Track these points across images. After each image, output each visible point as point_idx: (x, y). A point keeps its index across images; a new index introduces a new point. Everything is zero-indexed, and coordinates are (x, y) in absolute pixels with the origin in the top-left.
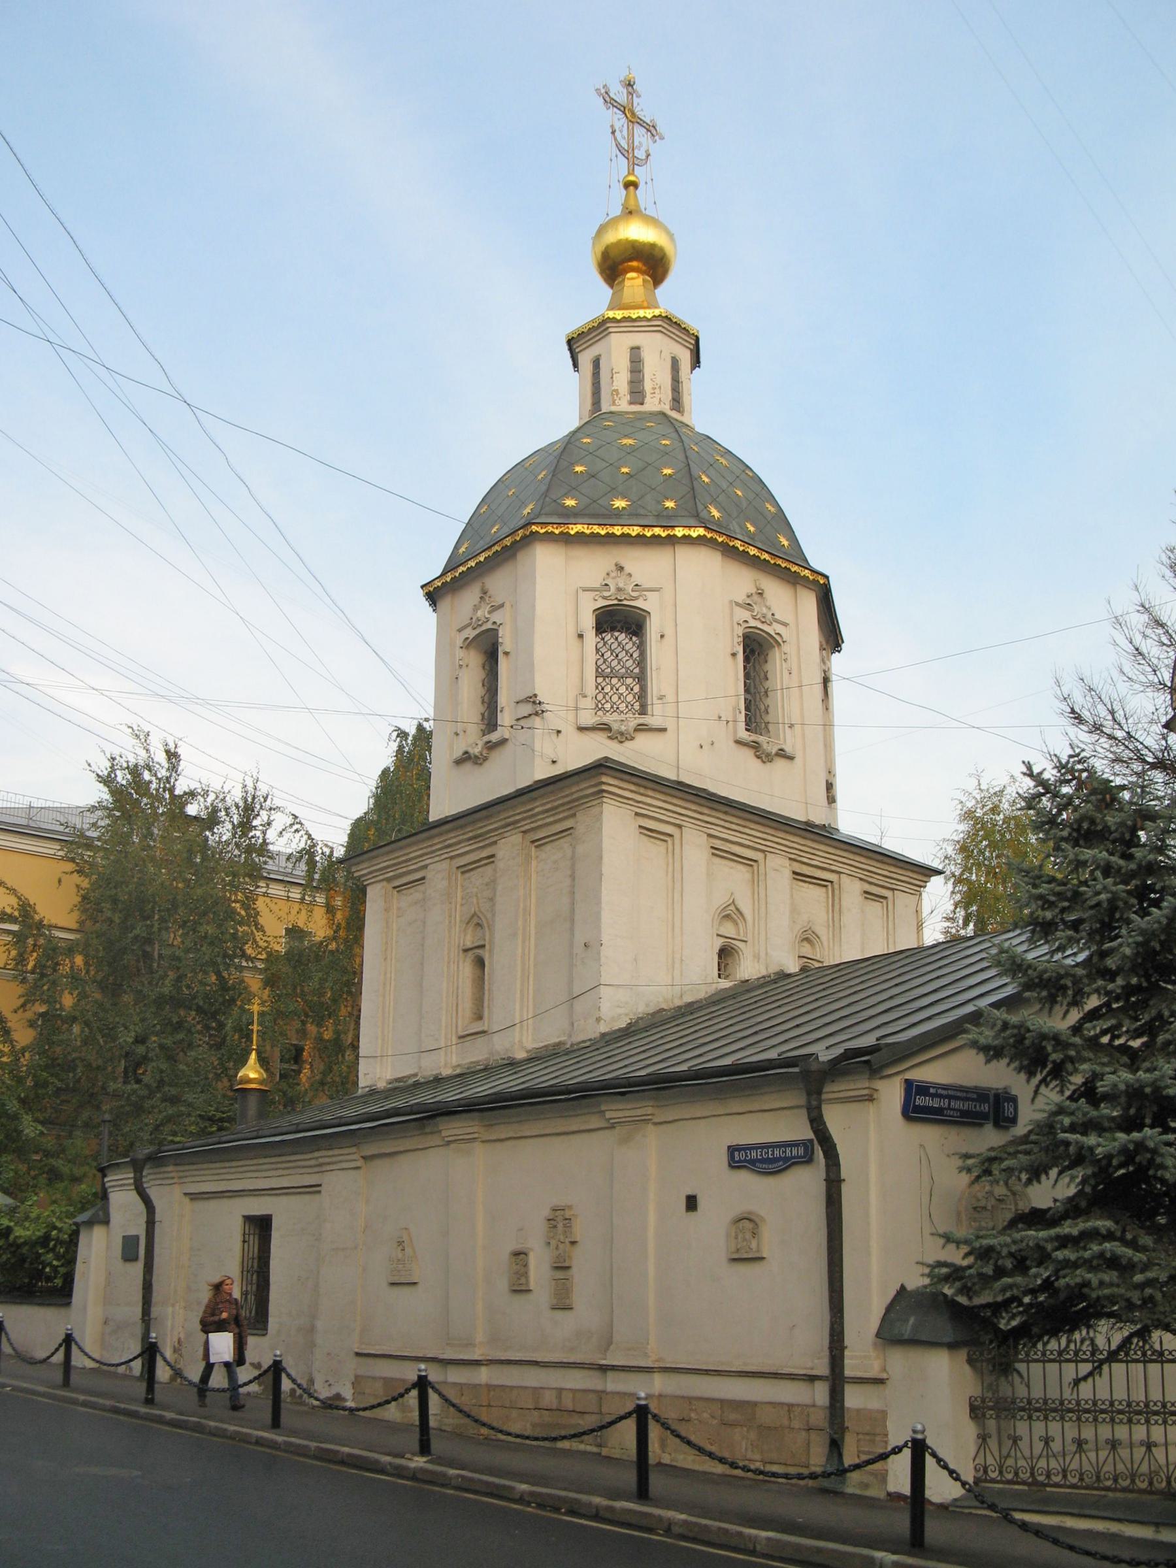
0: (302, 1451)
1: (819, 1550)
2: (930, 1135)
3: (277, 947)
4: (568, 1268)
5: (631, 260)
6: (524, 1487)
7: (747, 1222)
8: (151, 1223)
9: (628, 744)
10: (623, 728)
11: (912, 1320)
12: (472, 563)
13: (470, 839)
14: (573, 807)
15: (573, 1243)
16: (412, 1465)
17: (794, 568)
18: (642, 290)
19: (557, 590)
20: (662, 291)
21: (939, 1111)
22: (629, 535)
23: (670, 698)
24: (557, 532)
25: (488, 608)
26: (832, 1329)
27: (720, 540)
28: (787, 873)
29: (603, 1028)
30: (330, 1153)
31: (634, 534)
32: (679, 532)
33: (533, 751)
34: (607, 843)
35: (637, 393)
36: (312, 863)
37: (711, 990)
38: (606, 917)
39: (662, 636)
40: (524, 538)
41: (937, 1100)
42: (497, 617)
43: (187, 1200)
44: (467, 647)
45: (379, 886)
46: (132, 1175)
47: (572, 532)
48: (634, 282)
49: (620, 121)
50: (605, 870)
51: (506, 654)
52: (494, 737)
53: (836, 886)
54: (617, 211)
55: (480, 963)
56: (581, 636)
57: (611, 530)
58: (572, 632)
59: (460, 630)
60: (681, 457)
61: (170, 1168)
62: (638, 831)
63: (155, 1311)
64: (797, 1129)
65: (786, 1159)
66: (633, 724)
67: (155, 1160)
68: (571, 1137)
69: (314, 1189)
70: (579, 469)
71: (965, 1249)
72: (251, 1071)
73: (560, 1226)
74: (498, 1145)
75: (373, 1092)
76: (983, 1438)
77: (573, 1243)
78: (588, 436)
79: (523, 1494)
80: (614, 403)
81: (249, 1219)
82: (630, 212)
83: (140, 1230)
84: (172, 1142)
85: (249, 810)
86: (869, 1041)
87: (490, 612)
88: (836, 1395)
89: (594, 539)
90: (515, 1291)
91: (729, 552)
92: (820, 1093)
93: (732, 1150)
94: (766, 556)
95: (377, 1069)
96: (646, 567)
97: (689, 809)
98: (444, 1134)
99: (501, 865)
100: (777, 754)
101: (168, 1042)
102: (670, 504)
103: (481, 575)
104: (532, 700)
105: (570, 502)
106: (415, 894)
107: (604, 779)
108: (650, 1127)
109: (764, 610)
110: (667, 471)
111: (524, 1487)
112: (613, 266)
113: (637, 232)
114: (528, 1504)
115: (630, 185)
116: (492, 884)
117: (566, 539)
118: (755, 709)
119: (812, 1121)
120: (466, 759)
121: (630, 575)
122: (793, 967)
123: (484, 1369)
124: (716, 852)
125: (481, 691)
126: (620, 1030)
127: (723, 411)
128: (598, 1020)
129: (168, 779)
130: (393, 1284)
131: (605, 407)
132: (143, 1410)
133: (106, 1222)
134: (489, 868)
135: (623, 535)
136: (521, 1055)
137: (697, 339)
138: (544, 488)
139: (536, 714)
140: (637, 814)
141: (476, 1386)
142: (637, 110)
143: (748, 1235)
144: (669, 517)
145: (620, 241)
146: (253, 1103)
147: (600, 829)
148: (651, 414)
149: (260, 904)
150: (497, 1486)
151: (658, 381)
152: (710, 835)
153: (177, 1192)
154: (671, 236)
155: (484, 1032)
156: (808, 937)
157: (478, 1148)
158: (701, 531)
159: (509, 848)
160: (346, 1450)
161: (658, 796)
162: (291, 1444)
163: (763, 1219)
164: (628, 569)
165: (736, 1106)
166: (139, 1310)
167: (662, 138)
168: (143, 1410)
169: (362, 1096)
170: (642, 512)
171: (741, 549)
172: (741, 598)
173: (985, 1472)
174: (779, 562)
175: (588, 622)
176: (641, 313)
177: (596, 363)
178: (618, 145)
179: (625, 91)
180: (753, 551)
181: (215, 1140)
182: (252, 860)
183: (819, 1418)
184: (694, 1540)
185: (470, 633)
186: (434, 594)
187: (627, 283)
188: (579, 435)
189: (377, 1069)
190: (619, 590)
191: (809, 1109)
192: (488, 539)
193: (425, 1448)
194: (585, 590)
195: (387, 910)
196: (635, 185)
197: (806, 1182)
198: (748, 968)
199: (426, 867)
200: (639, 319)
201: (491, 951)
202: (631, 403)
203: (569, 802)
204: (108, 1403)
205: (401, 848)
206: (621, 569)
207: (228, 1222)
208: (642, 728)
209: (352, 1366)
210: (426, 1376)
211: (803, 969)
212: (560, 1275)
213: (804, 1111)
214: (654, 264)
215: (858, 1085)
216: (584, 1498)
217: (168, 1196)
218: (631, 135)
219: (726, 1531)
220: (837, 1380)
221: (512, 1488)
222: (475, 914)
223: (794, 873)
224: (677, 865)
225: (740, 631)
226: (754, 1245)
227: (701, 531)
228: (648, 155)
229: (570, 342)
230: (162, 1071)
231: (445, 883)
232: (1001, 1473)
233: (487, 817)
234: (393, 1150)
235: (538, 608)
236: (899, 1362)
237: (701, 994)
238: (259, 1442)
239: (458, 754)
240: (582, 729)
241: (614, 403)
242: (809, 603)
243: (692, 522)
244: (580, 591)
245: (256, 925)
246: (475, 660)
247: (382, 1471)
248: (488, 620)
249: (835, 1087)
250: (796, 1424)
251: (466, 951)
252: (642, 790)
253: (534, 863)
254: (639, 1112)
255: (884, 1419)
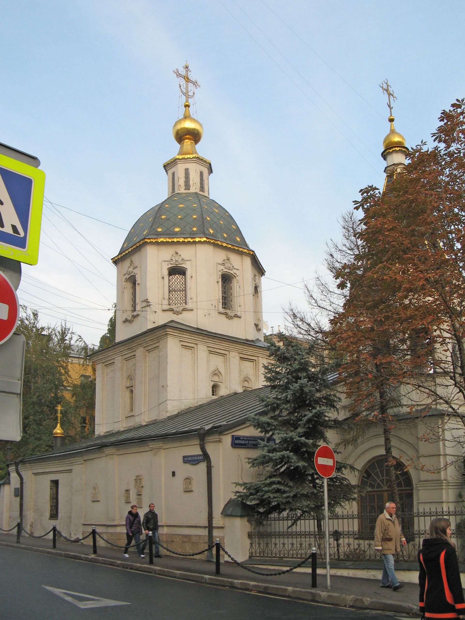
0: (60, 555)
1: (191, 576)
2: (243, 453)
3: (76, 383)
4: (141, 495)
5: (186, 135)
6: (119, 562)
7: (188, 480)
8: (22, 483)
9: (180, 315)
10: (178, 310)
11: (231, 509)
12: (127, 252)
13: (127, 349)
14: (159, 339)
15: (142, 487)
16: (90, 557)
17: (241, 249)
18: (190, 146)
19: (155, 261)
20: (198, 147)
21: (245, 445)
22: (179, 241)
23: (194, 299)
24: (154, 241)
25: (132, 268)
26: (20, 503)
27: (212, 242)
28: (238, 358)
29: (168, 414)
30: (74, 459)
31: (181, 241)
32: (197, 240)
33: (147, 319)
34: (169, 352)
35: (187, 186)
36: (86, 352)
37: (209, 400)
38: (169, 377)
39: (191, 277)
40: (143, 243)
41: (243, 441)
42: (135, 271)
43: (33, 475)
44: (127, 281)
45: (100, 365)
46: (15, 467)
47: (159, 241)
48: (187, 143)
49: (183, 82)
50: (169, 361)
51: (139, 284)
52: (135, 313)
53: (257, 361)
54: (182, 117)
55: (132, 391)
56: (163, 278)
57: (173, 240)
58: (160, 277)
59: (124, 275)
60: (200, 211)
61: (27, 465)
62: (181, 347)
63: (24, 513)
64: (198, 451)
65: (198, 460)
66: (181, 308)
67: (23, 462)
68: (142, 453)
69: (70, 471)
70: (163, 217)
71: (243, 487)
72: (58, 430)
73: (138, 481)
74: (121, 456)
75: (100, 437)
76: (251, 544)
77: (142, 487)
78: (167, 204)
79: (119, 564)
80: (179, 190)
81: (52, 481)
82: (186, 117)
83: (19, 486)
84: (36, 455)
85: (63, 333)
86: (199, 427)
87: (133, 269)
88: (210, 532)
89: (167, 243)
90: (127, 503)
91: (216, 245)
92: (203, 440)
93: (184, 457)
94: (230, 246)
95: (101, 429)
96: (186, 253)
97: (199, 338)
98: (106, 452)
99: (137, 358)
100: (234, 316)
101: (37, 418)
102: (195, 229)
103: (130, 256)
104: (146, 301)
105: (160, 230)
106: (111, 368)
107: (167, 330)
108: (162, 450)
109: (229, 265)
110: (195, 217)
111: (119, 562)
112: (181, 136)
113: (188, 125)
114: (120, 567)
115: (187, 106)
116: (135, 365)
117: (157, 243)
118: (226, 301)
119: (201, 449)
120: (126, 321)
121: (180, 255)
122: (240, 390)
123: (118, 528)
124: (211, 352)
125: (132, 297)
126: (175, 415)
127: (220, 191)
128: (167, 412)
129: (34, 323)
130: (93, 501)
131: (177, 191)
132: (16, 545)
133: (9, 483)
134: (134, 360)
135: (177, 241)
136: (144, 424)
137: (210, 164)
138: (151, 224)
139: (148, 306)
140: (180, 341)
141: (116, 533)
142: (190, 77)
143: (188, 484)
144: (194, 234)
145: (182, 128)
146: (59, 441)
147: (167, 347)
148: (193, 193)
149: (70, 367)
150: (112, 562)
151: (195, 181)
152: (208, 346)
153: (30, 473)
154: (201, 125)
155: (133, 416)
156: (246, 380)
157: (115, 457)
158: (205, 239)
159: (140, 352)
160: (73, 554)
161: (187, 334)
162: (57, 553)
163: (192, 479)
164: (179, 253)
165: (185, 443)
166: (19, 513)
167: (199, 87)
168: (16, 545)
169: (96, 438)
170: (185, 232)
171: (220, 244)
172: (221, 261)
173: (252, 554)
174: (235, 248)
175: (166, 273)
176: (189, 156)
177: (173, 174)
178: (182, 91)
179: (185, 70)
180: (224, 245)
181: (52, 453)
182: (66, 350)
183: (206, 539)
184: (162, 575)
185: (127, 276)
186: (116, 261)
187: (185, 144)
188: (164, 204)
189: (101, 429)
190: (176, 261)
191: (200, 445)
192: (133, 242)
193: (95, 552)
194: (164, 261)
195: (103, 373)
196: (188, 106)
197: (203, 466)
198: (223, 392)
199: (114, 358)
200: (188, 158)
201: (135, 388)
202: (185, 189)
203: (158, 337)
204: (5, 543)
205: (106, 352)
206: (177, 253)
207: (46, 481)
208: (184, 310)
209: (81, 529)
210: (95, 530)
211: (245, 391)
212: (139, 497)
213: (199, 446)
214: (195, 136)
215: (215, 437)
216: (135, 564)
217: (27, 474)
218: (187, 87)
219: (169, 572)
220: (210, 527)
221: (116, 562)
222: (130, 375)
223: (241, 358)
224: (196, 358)
225: (220, 274)
226: (190, 486)
227: (205, 239)
228: (194, 94)
229: (165, 166)
230: (34, 429)
231: (120, 364)
232: (272, 554)
233: (133, 342)
234: (92, 458)
235: (148, 268)
236: (228, 522)
237: (205, 401)
238: (48, 553)
239: (124, 319)
240: (163, 311)
241: (179, 190)
242: (248, 261)
243: (202, 235)
244: (163, 262)
245: (68, 375)
246: (129, 285)
247: (82, 559)
248: (132, 272)
249: (210, 438)
250: (201, 542)
251: (127, 388)
252: (181, 333)
253: (147, 358)
254: (159, 445)
255: (224, 539)
